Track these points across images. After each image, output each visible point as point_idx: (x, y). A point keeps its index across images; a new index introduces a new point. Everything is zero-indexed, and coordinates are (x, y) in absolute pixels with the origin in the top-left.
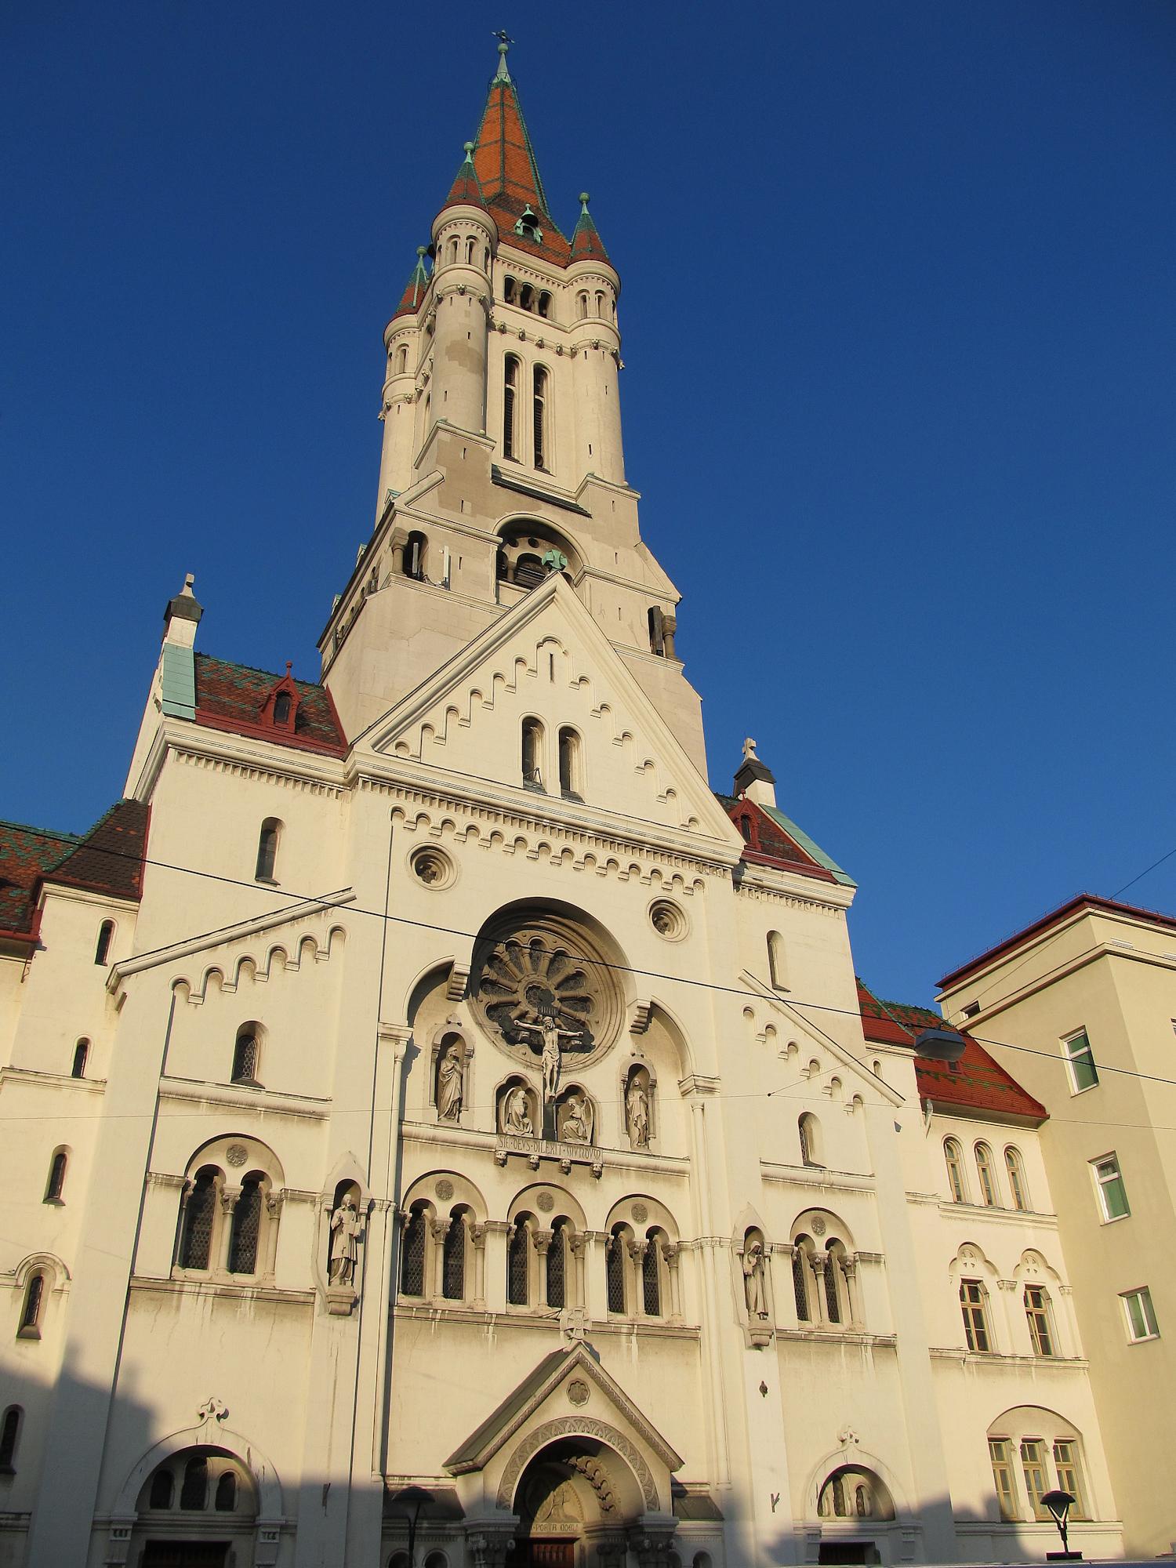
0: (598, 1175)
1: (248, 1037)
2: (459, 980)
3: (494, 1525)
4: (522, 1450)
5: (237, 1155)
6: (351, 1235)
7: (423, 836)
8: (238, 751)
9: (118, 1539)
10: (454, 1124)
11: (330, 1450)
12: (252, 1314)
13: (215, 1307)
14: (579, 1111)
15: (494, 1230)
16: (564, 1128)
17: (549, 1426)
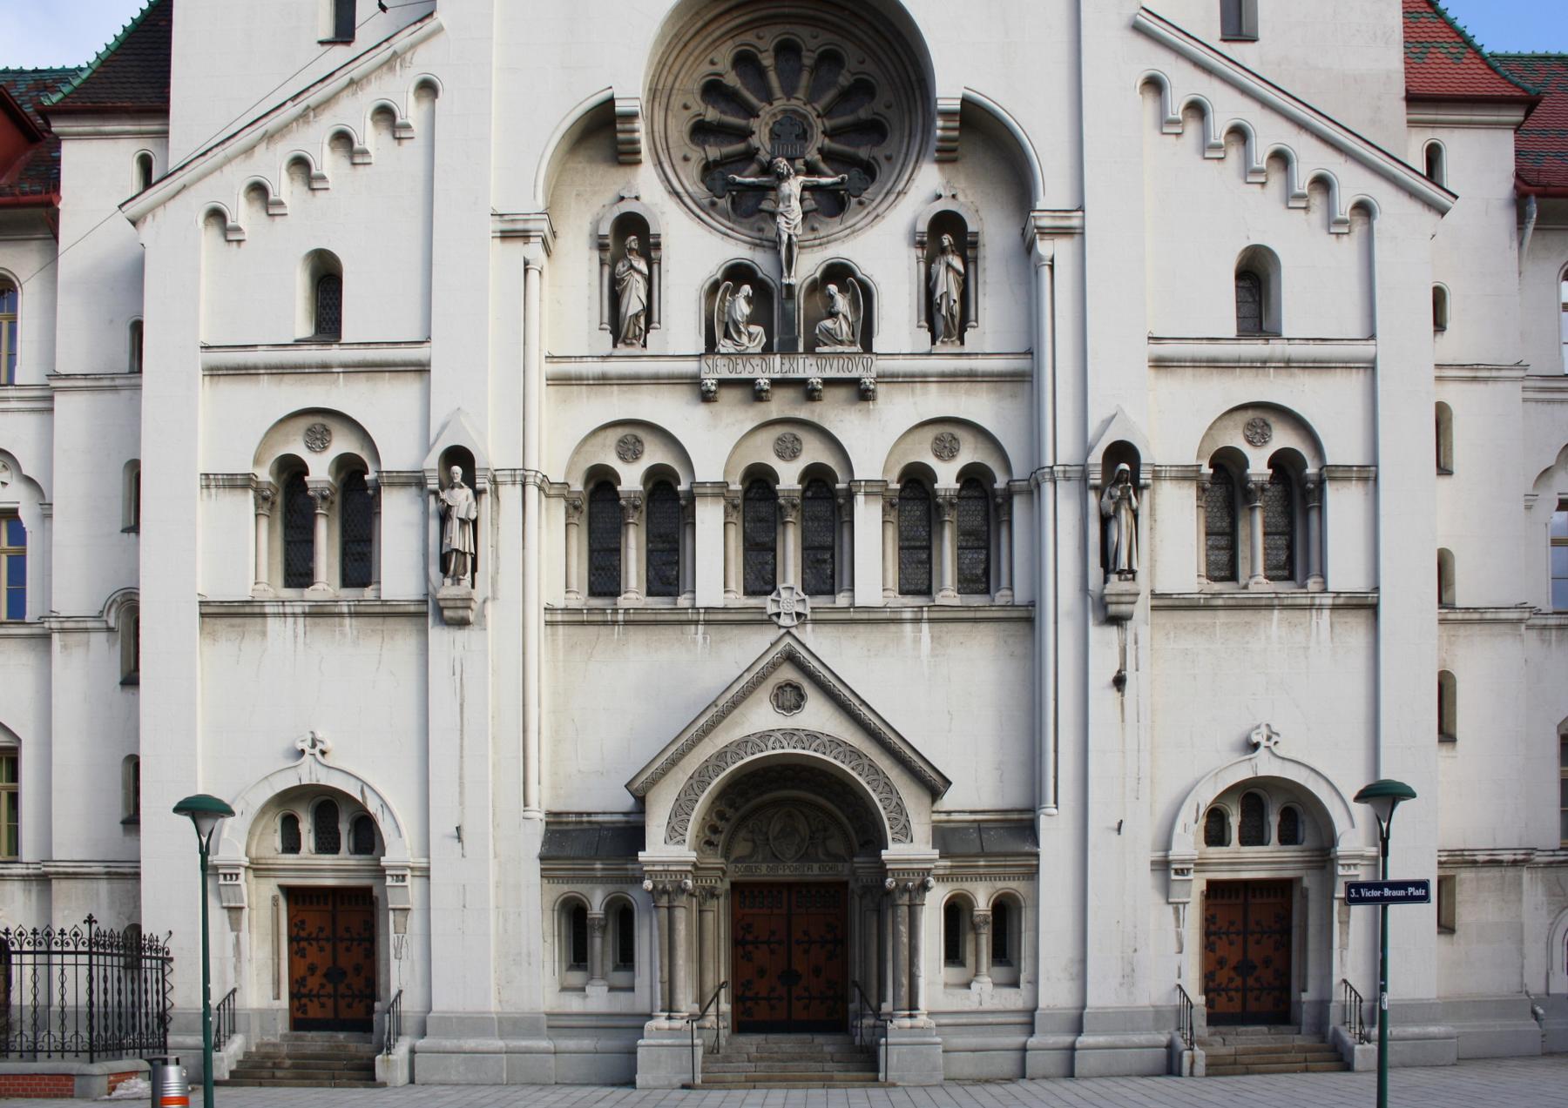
3: (663, 863)
4: (699, 779)
9: (228, 883)
11: (461, 785)
12: (355, 633)
13: (308, 628)
14: (842, 303)
15: (704, 495)
16: (817, 331)
17: (745, 742)
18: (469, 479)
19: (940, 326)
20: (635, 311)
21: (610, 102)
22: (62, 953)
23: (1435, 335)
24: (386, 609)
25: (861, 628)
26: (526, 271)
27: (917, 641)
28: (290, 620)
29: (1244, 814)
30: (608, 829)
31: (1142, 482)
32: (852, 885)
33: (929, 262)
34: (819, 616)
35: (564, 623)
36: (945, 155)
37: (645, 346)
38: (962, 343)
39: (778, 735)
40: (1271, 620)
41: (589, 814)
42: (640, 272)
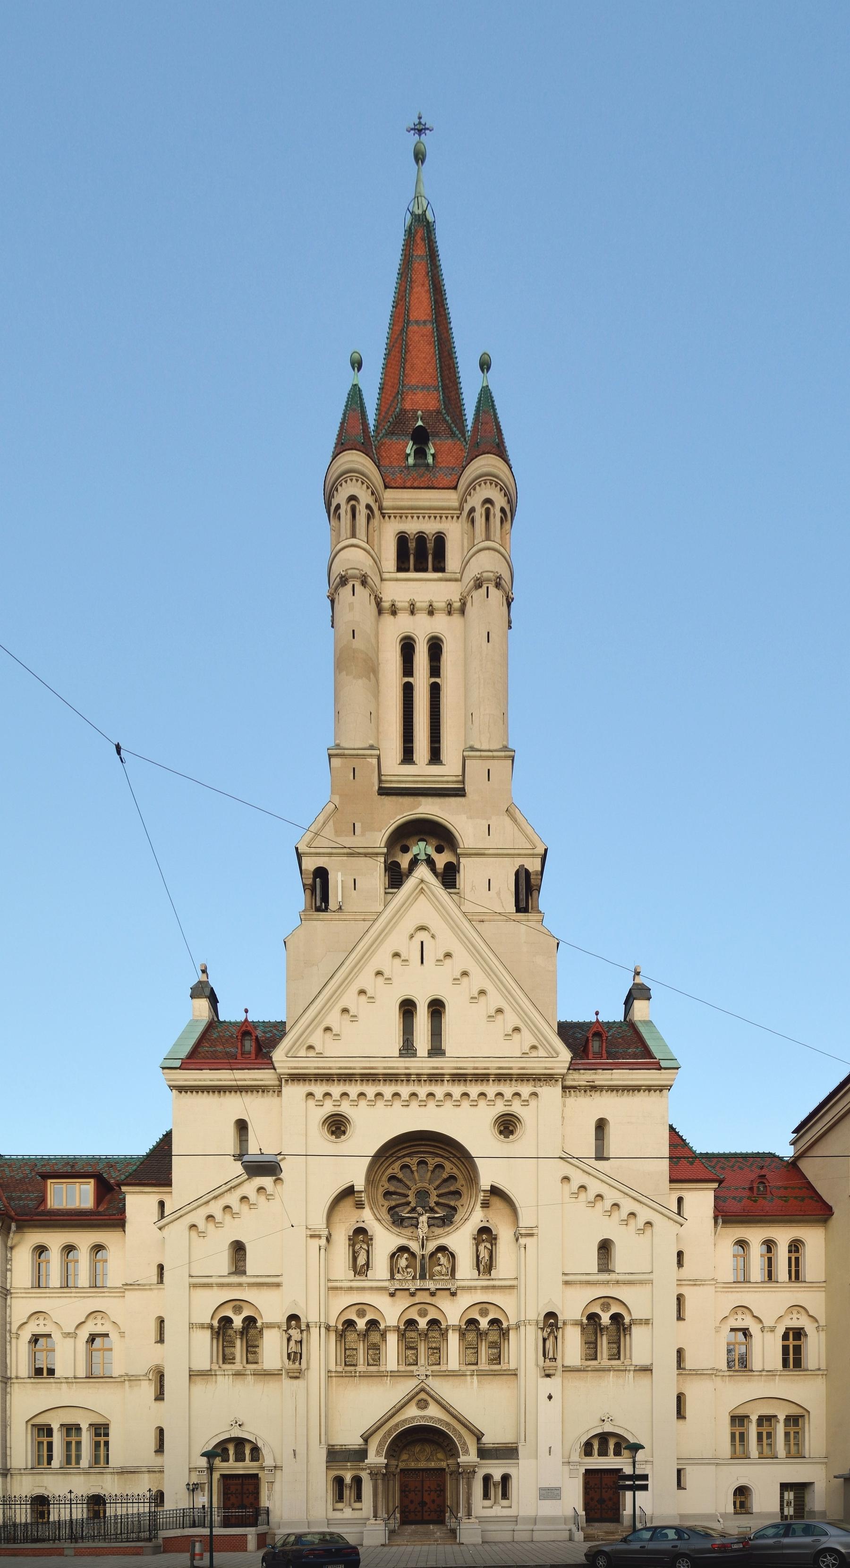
0: (454, 1294)
1: (239, 1249)
2: (359, 1195)
3: (374, 1464)
4: (389, 1432)
5: (238, 1310)
6: (296, 1341)
7: (329, 1108)
8: (211, 1080)
10: (363, 1278)
14: (443, 1260)
17: (405, 1421)
18: (298, 1326)
19: (482, 1268)
20: (363, 1264)
21: (352, 1186)
22: (15, 1504)
23: (679, 1268)
24: (266, 1373)
25: (450, 1378)
26: (320, 1249)
27: (472, 1382)
28: (227, 1377)
29: (599, 1445)
30: (352, 1451)
31: (559, 1326)
32: (447, 1470)
33: (477, 1245)
34: (434, 1374)
35: (335, 1376)
36: (484, 1205)
37: (366, 1276)
38: (490, 1275)
39: (419, 1418)
40: (610, 1375)
41: (345, 1445)
42: (364, 1249)
